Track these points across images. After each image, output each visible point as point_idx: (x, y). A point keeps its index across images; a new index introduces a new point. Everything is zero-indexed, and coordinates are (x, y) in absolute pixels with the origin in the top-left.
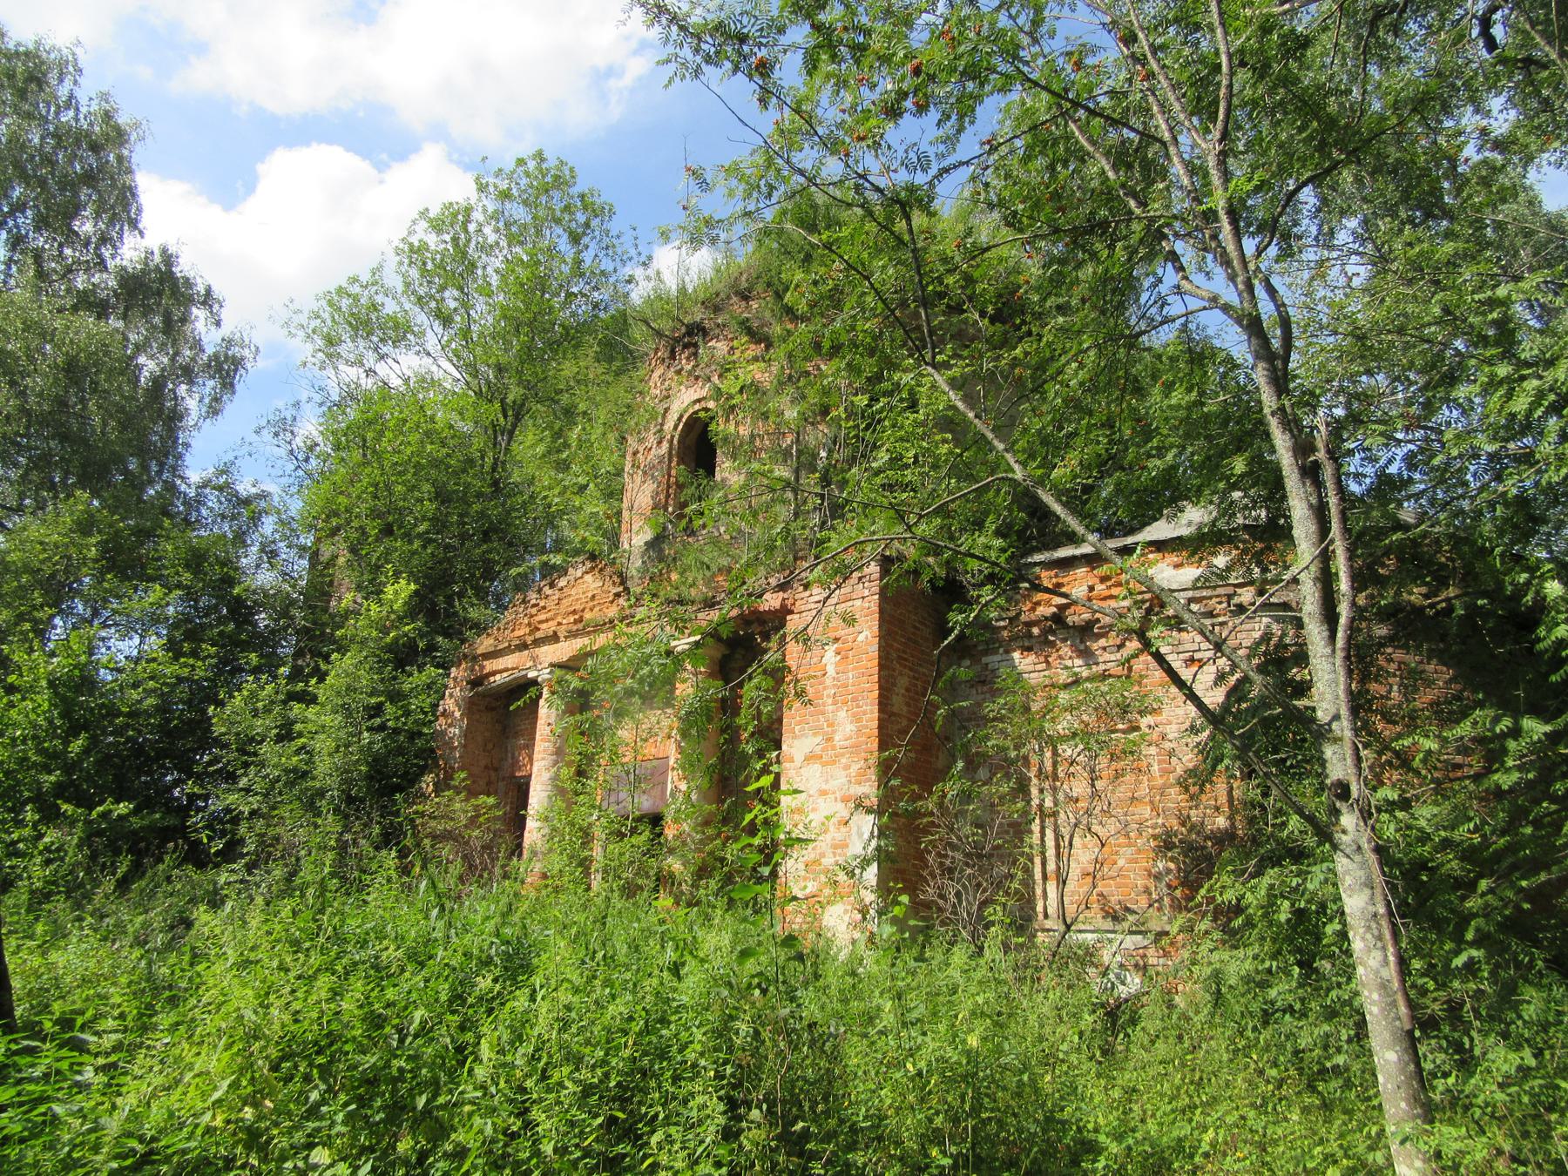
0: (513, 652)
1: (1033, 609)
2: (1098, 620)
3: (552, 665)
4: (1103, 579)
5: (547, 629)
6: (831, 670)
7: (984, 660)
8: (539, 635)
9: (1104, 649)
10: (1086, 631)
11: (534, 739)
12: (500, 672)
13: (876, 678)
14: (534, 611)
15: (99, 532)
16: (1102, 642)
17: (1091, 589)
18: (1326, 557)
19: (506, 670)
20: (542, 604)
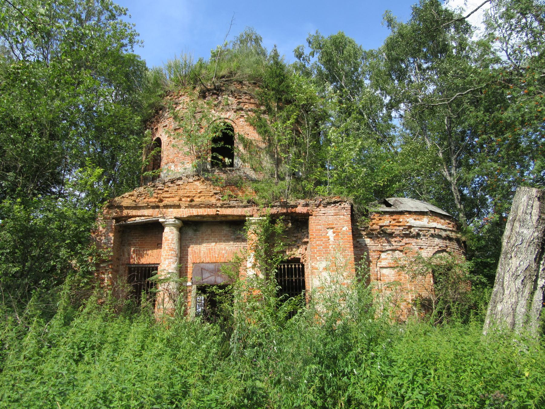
0: (149, 208)
1: (372, 226)
2: (394, 233)
3: (175, 218)
4: (394, 220)
5: (166, 202)
6: (332, 239)
7: (358, 240)
8: (193, 203)
9: (395, 241)
10: (391, 235)
11: (162, 240)
12: (139, 216)
13: (352, 244)
14: (160, 192)
15: (306, 327)
16: (395, 239)
17: (390, 222)
18: (144, 216)
19: (144, 216)
20: (166, 189)
